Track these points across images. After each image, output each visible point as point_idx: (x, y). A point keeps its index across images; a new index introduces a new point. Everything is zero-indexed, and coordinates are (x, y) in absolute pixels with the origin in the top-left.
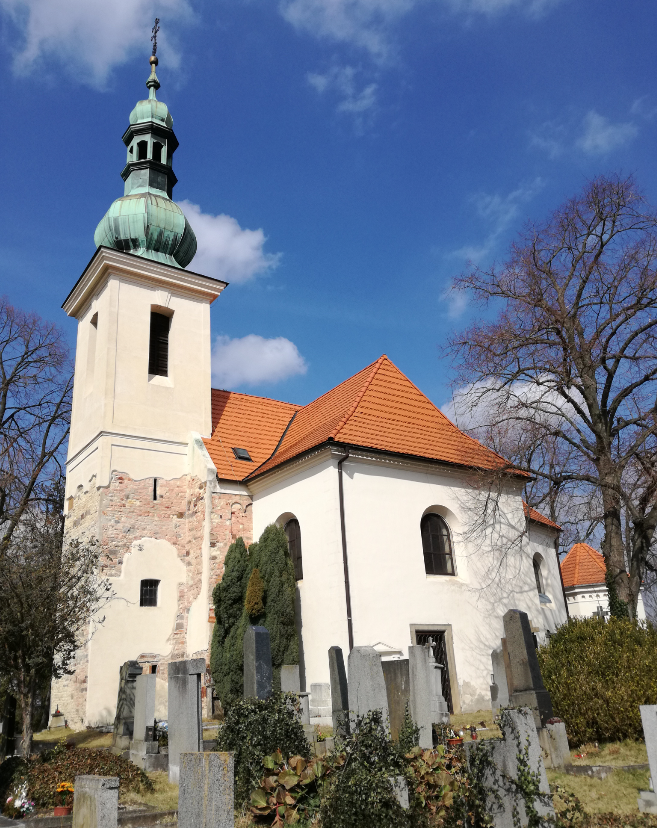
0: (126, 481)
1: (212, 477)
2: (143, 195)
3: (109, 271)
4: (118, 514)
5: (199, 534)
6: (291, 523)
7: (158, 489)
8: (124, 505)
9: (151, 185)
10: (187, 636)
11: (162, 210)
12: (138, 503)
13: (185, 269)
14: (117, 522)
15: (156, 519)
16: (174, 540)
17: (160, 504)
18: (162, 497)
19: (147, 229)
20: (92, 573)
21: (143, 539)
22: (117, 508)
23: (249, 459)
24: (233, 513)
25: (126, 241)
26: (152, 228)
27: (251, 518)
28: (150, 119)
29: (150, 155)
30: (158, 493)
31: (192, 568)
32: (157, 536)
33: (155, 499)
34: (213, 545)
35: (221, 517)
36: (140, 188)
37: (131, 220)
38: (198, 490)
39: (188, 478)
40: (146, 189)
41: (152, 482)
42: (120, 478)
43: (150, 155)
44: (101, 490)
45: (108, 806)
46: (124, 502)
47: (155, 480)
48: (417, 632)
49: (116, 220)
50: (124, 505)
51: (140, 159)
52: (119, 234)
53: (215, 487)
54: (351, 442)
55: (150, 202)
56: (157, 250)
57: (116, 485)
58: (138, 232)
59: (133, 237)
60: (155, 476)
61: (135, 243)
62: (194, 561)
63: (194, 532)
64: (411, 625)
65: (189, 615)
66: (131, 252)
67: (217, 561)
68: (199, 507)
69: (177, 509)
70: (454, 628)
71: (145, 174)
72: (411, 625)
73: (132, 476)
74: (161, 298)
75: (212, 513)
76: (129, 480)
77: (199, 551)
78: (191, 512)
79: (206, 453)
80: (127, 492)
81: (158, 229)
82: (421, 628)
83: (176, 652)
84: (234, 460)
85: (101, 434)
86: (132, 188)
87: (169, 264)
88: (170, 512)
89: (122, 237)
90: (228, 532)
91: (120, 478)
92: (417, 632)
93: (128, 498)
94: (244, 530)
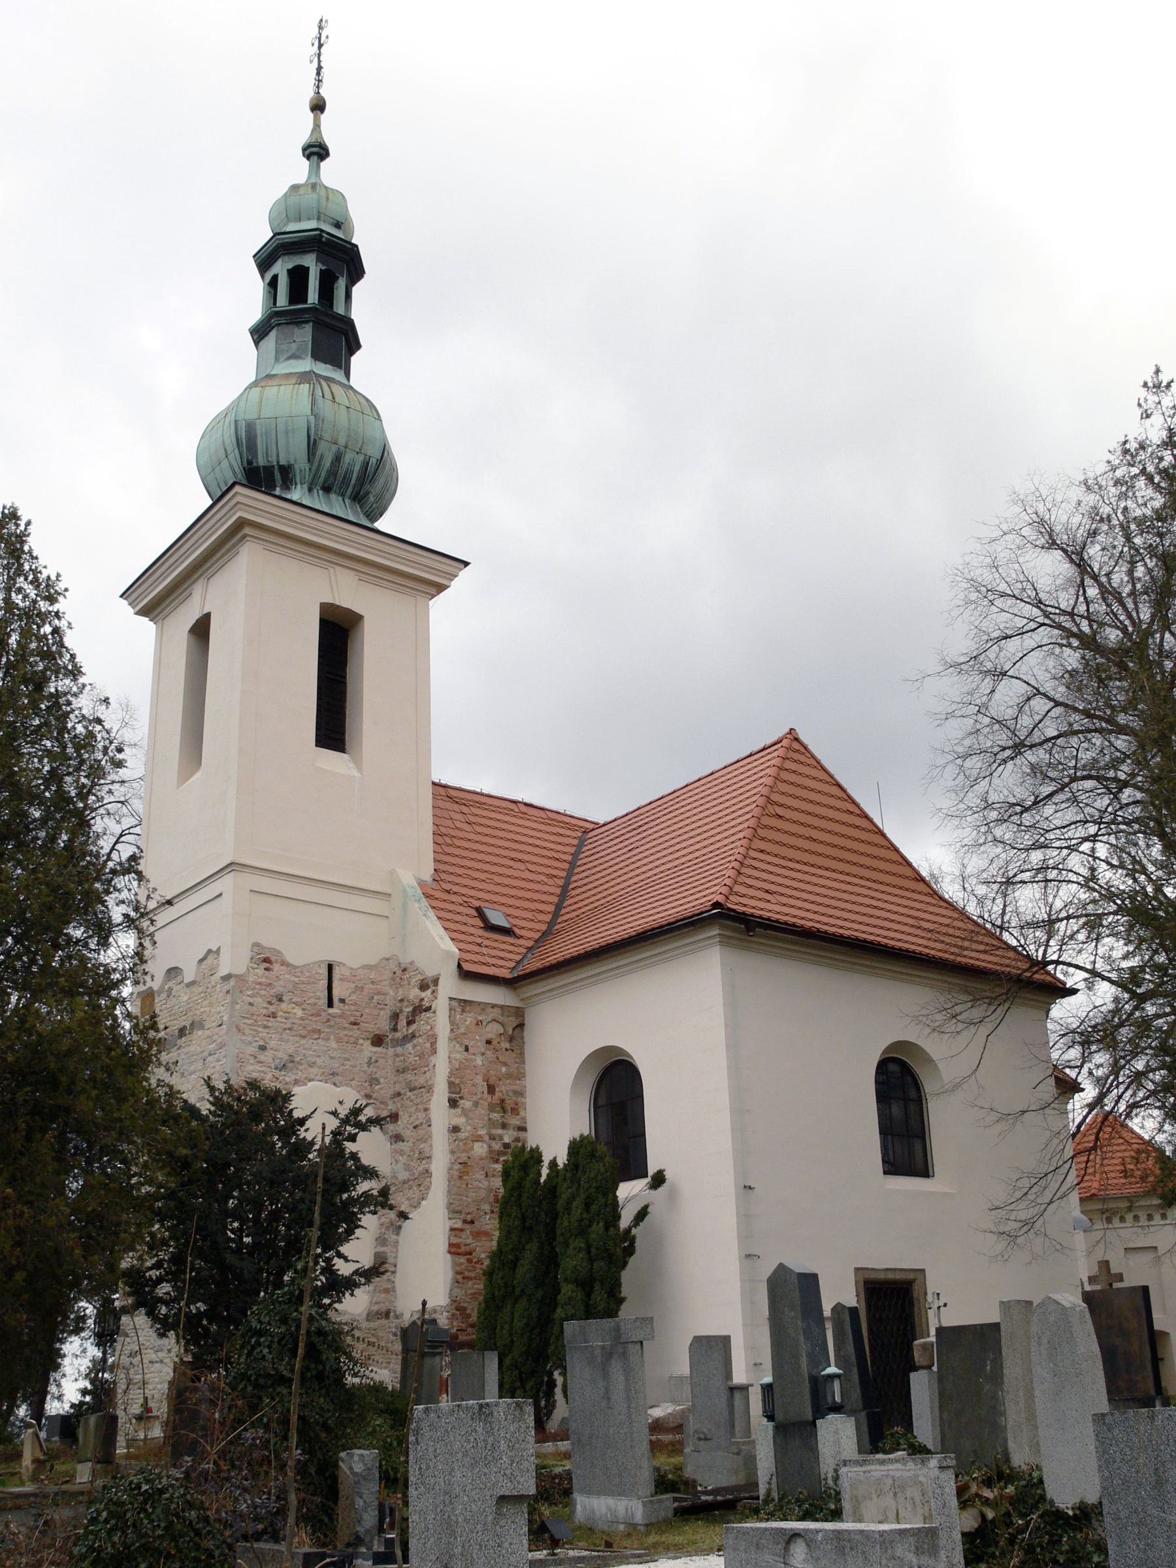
0: (276, 967)
2: (304, 377)
3: (247, 530)
4: (263, 1033)
5: (421, 1080)
7: (335, 984)
8: (274, 1015)
9: (317, 356)
10: (398, 1279)
11: (343, 410)
12: (299, 1012)
13: (288, 496)
14: (263, 1048)
15: (334, 1045)
16: (368, 1091)
17: (340, 1016)
18: (342, 1001)
19: (312, 447)
21: (310, 1084)
22: (262, 1021)
24: (489, 1042)
25: (269, 470)
26: (322, 447)
28: (312, 224)
29: (313, 297)
30: (335, 992)
31: (405, 1146)
32: (337, 1079)
33: (330, 1004)
34: (453, 1103)
35: (467, 1049)
37: (281, 428)
38: (416, 991)
39: (392, 966)
40: (306, 364)
41: (324, 971)
42: (267, 960)
43: (313, 297)
44: (232, 982)
45: (947, 1490)
46: (272, 1009)
47: (330, 968)
48: (866, 1282)
50: (274, 1015)
52: (255, 455)
55: (319, 393)
56: (327, 489)
58: (294, 452)
60: (330, 958)
62: (407, 1133)
63: (409, 1076)
64: (858, 1270)
65: (401, 1238)
67: (462, 1135)
68: (421, 1025)
70: (933, 1284)
72: (857, 1270)
73: (290, 959)
76: (284, 963)
77: (421, 1115)
78: (399, 1035)
80: (278, 988)
81: (334, 448)
82: (873, 1276)
83: (375, 1308)
84: (481, 932)
85: (490, 927)
89: (261, 461)
90: (479, 1080)
91: (267, 960)
92: (866, 1282)
93: (280, 1000)
94: (509, 1076)
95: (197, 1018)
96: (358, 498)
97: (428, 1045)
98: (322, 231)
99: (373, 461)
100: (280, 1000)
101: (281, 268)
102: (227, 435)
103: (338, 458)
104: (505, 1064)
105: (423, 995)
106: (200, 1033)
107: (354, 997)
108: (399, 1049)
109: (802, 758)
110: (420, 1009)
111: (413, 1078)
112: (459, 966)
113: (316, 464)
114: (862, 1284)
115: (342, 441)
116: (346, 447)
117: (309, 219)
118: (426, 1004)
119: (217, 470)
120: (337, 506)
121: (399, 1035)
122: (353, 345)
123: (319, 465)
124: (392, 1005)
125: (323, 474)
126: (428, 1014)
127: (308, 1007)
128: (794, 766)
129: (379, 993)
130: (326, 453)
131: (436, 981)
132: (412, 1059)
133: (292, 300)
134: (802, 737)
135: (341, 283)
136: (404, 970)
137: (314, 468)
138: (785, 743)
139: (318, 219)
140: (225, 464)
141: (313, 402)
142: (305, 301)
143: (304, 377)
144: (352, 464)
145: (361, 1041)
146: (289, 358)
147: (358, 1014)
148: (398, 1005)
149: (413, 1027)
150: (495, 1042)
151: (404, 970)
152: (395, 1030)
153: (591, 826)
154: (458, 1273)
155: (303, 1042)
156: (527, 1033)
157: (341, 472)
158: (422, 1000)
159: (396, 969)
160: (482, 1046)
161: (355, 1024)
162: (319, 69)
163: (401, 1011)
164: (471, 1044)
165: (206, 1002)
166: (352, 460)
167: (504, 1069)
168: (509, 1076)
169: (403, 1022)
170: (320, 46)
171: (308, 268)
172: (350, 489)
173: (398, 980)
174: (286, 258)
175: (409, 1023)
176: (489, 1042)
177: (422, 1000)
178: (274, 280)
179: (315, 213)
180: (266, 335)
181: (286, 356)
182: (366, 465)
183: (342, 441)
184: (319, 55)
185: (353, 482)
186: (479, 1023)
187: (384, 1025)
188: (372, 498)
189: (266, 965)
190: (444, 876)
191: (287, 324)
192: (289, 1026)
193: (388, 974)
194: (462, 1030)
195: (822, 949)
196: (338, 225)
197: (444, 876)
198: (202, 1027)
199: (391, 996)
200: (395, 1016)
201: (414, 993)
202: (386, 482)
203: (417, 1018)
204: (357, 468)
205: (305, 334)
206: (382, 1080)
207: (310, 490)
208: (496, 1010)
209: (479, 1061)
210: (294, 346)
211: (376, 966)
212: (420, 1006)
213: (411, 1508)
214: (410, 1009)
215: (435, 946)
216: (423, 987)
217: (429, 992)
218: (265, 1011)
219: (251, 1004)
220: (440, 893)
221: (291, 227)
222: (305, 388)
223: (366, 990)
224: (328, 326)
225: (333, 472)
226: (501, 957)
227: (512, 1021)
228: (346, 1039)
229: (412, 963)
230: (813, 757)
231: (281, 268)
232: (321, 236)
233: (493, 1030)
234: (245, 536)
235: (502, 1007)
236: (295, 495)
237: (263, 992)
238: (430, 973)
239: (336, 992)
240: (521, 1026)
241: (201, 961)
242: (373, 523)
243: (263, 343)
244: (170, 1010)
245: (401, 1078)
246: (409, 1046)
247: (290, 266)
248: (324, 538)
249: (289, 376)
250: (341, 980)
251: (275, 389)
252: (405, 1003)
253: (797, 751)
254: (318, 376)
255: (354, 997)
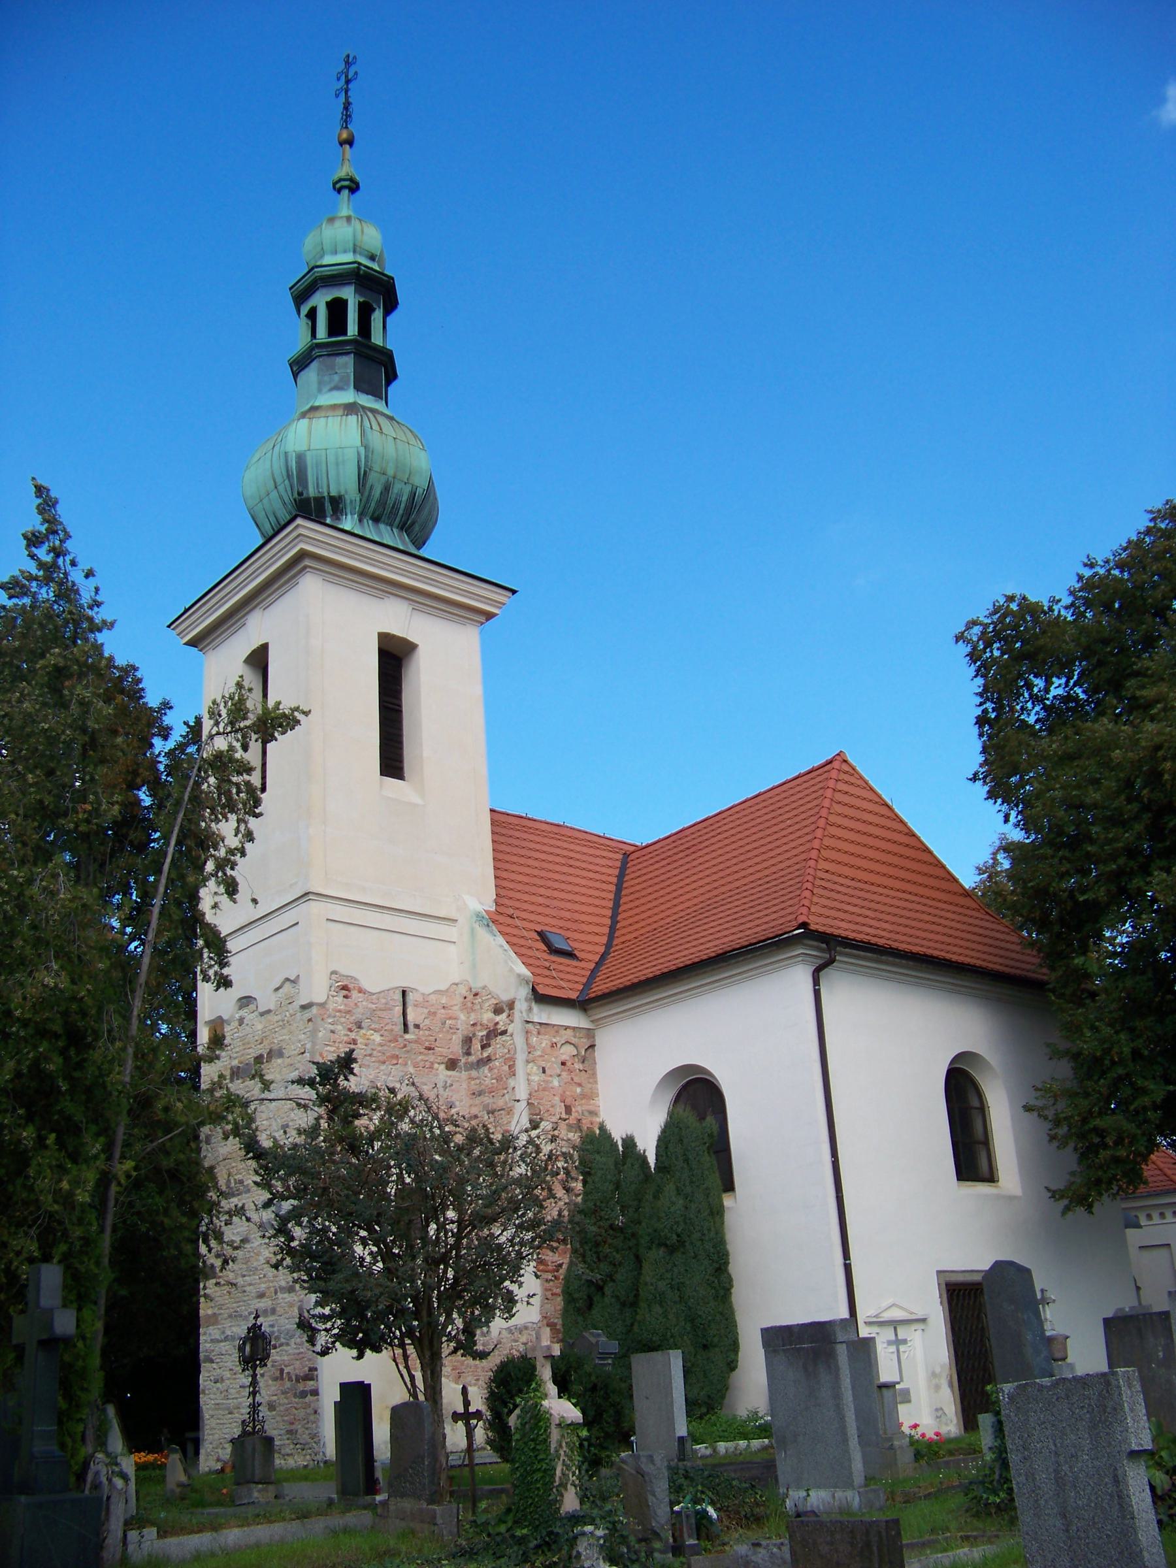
0: (354, 994)
1: (524, 992)
2: (351, 409)
3: (307, 562)
5: (500, 1103)
6: (697, 1097)
7: (409, 1010)
9: (358, 388)
11: (390, 440)
12: (377, 1038)
13: (421, 553)
17: (416, 1042)
18: (417, 1026)
19: (363, 478)
20: (257, 1173)
23: (570, 955)
24: (563, 1064)
25: (319, 501)
26: (373, 478)
27: (594, 1075)
28: (349, 257)
29: (352, 329)
30: (410, 1018)
33: (406, 1030)
35: (544, 1072)
36: (336, 393)
37: (331, 459)
38: (490, 1015)
39: (462, 990)
40: (349, 396)
41: (399, 997)
43: (352, 329)
46: (353, 1035)
48: (947, 1285)
49: (301, 458)
51: (330, 334)
52: (306, 487)
53: (530, 1009)
54: (836, 932)
56: (376, 520)
57: (338, 1002)
58: (345, 483)
59: (333, 494)
61: (337, 504)
63: (487, 1099)
64: (939, 1272)
66: (328, 521)
68: (498, 1047)
69: (444, 1051)
71: (345, 365)
72: (939, 1272)
73: (366, 985)
74: (397, 619)
75: (528, 1062)
76: (360, 991)
78: (472, 1059)
79: (501, 940)
80: (358, 1015)
81: (383, 479)
86: (320, 391)
87: (369, 536)
88: (432, 1058)
89: (312, 492)
91: (345, 988)
93: (360, 1027)
94: (584, 1096)
95: (275, 1047)
96: (405, 527)
97: (506, 1068)
98: (359, 264)
99: (420, 491)
100: (360, 1027)
101: (320, 300)
102: (276, 466)
103: (387, 488)
104: (580, 1085)
105: (498, 1018)
106: (279, 1061)
107: (427, 1022)
108: (474, 1073)
109: (852, 780)
110: (494, 1033)
111: (491, 1101)
112: (534, 989)
113: (366, 494)
114: (944, 1286)
115: (391, 472)
116: (394, 478)
117: (345, 252)
118: (501, 1027)
119: (265, 501)
120: (387, 535)
121: (472, 1059)
122: (392, 376)
123: (369, 496)
124: (463, 1029)
125: (373, 505)
126: (504, 1038)
127: (386, 1033)
128: (845, 787)
129: (450, 1018)
130: (376, 484)
131: (511, 1005)
132: (488, 1081)
133: (331, 333)
134: (849, 759)
135: (377, 316)
136: (476, 995)
137: (364, 499)
138: (836, 765)
139: (354, 252)
140: (274, 495)
141: (363, 433)
142: (345, 333)
143: (351, 409)
144: (400, 495)
145: (436, 1066)
146: (331, 390)
147: (433, 1039)
148: (472, 1029)
149: (490, 1050)
150: (569, 1064)
151: (476, 995)
152: (468, 1053)
153: (632, 849)
154: (546, 1290)
155: (383, 1067)
156: (598, 1053)
157: (390, 502)
158: (497, 1023)
159: (467, 994)
160: (558, 1069)
161: (430, 1049)
162: (347, 106)
163: (474, 1035)
164: (547, 1066)
165: (285, 1031)
166: (401, 492)
167: (579, 1090)
168: (584, 1096)
169: (476, 1045)
170: (348, 82)
171: (346, 301)
172: (398, 519)
173: (469, 1004)
174: (324, 291)
175: (483, 1047)
176: (563, 1064)
177: (497, 1023)
178: (312, 315)
179: (351, 245)
180: (306, 366)
181: (328, 387)
182: (413, 495)
183: (391, 472)
184: (347, 92)
185: (401, 512)
186: (553, 1045)
187: (455, 1048)
188: (417, 528)
189: (345, 992)
190: (506, 901)
191: (328, 355)
192: (369, 1052)
193: (459, 1000)
194: (539, 1053)
195: (893, 964)
196: (372, 258)
197: (506, 901)
198: (280, 1054)
199: (463, 1020)
200: (468, 1041)
201: (487, 1016)
202: (430, 512)
203: (493, 1042)
204: (405, 498)
205: (346, 364)
206: (457, 1103)
207: (360, 521)
208: (569, 1032)
209: (556, 1083)
210: (336, 378)
211: (447, 990)
212: (495, 1030)
213: (1012, 1472)
214: (484, 1033)
215: (504, 970)
216: (498, 1011)
217: (504, 1016)
218: (345, 1038)
219: (333, 1032)
220: (502, 918)
221: (328, 260)
222: (353, 419)
223: (439, 1016)
224: (368, 357)
225: (382, 502)
226: (569, 983)
227: (584, 1043)
228: (422, 1064)
229: (484, 987)
230: (861, 778)
231: (320, 300)
232: (358, 268)
233: (567, 1052)
234: (305, 567)
235: (574, 1028)
236: (348, 523)
237: (343, 1020)
238: (505, 997)
239: (411, 1018)
240: (592, 1046)
241: (277, 989)
242: (419, 549)
243: (303, 376)
244: (242, 1038)
245: (478, 1100)
246: (486, 1069)
247: (329, 298)
248: (374, 566)
249: (334, 407)
250: (416, 1006)
251: (323, 420)
252: (479, 1027)
253: (846, 773)
254: (364, 408)
255: (427, 1022)
